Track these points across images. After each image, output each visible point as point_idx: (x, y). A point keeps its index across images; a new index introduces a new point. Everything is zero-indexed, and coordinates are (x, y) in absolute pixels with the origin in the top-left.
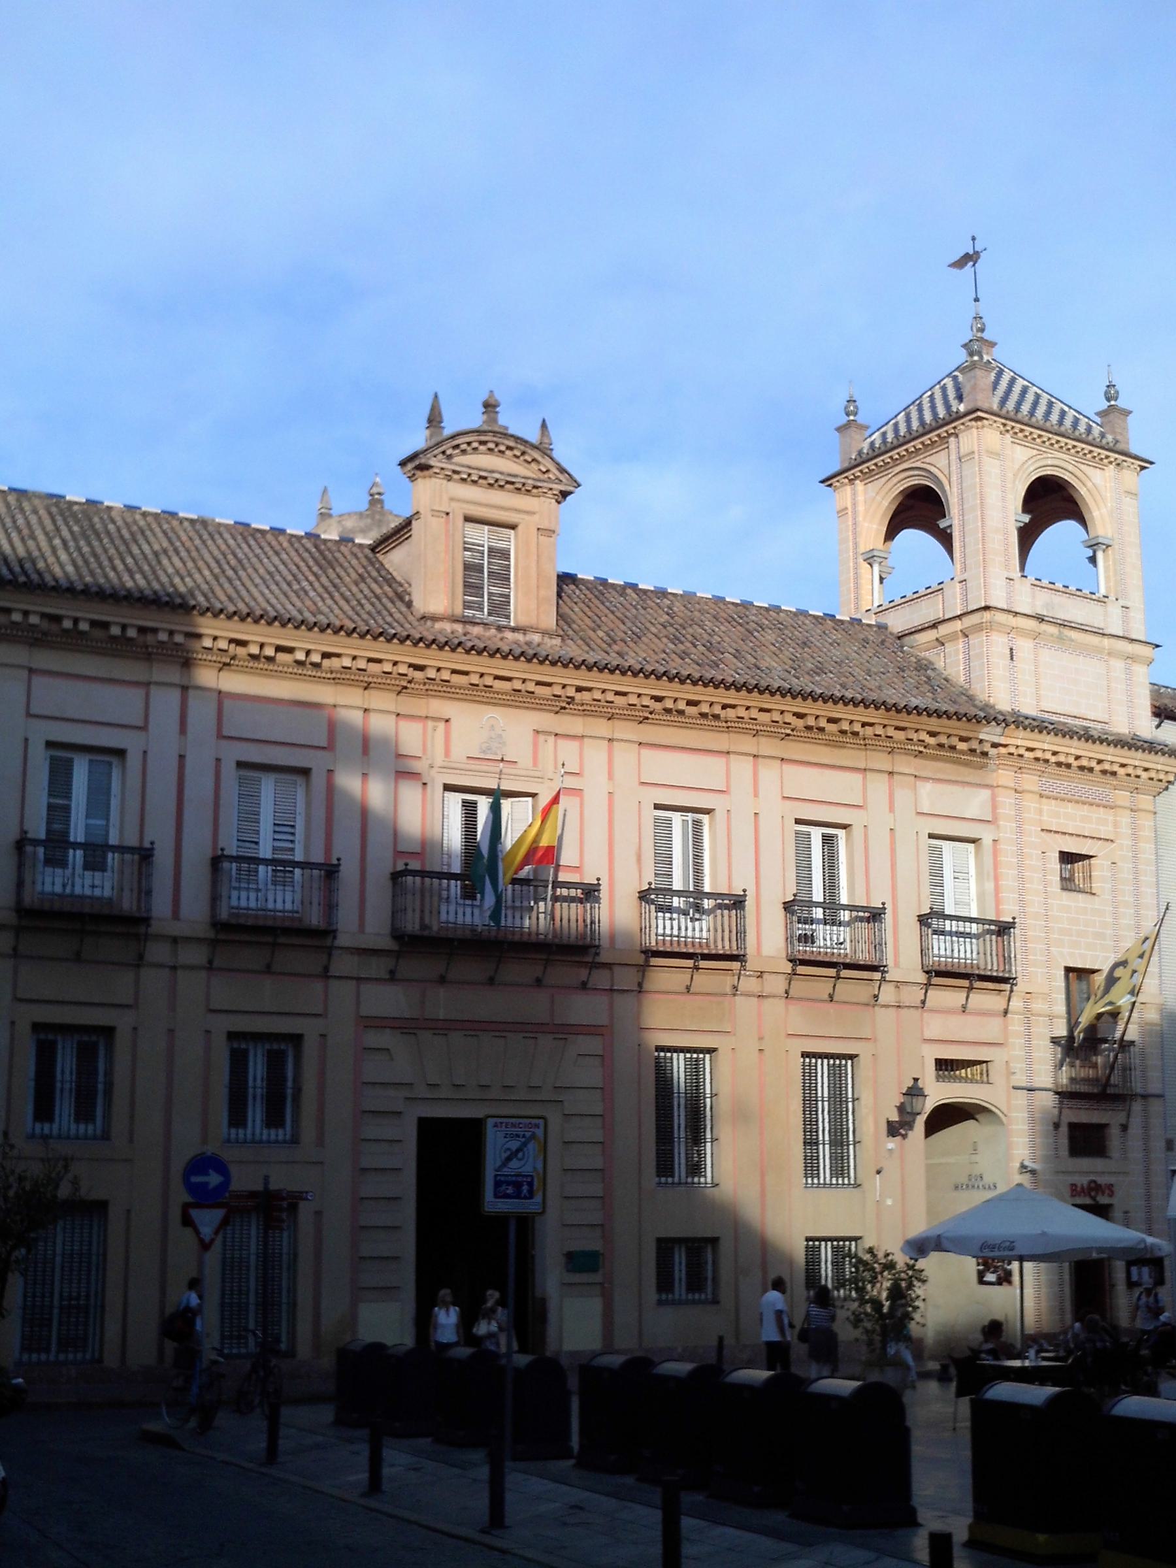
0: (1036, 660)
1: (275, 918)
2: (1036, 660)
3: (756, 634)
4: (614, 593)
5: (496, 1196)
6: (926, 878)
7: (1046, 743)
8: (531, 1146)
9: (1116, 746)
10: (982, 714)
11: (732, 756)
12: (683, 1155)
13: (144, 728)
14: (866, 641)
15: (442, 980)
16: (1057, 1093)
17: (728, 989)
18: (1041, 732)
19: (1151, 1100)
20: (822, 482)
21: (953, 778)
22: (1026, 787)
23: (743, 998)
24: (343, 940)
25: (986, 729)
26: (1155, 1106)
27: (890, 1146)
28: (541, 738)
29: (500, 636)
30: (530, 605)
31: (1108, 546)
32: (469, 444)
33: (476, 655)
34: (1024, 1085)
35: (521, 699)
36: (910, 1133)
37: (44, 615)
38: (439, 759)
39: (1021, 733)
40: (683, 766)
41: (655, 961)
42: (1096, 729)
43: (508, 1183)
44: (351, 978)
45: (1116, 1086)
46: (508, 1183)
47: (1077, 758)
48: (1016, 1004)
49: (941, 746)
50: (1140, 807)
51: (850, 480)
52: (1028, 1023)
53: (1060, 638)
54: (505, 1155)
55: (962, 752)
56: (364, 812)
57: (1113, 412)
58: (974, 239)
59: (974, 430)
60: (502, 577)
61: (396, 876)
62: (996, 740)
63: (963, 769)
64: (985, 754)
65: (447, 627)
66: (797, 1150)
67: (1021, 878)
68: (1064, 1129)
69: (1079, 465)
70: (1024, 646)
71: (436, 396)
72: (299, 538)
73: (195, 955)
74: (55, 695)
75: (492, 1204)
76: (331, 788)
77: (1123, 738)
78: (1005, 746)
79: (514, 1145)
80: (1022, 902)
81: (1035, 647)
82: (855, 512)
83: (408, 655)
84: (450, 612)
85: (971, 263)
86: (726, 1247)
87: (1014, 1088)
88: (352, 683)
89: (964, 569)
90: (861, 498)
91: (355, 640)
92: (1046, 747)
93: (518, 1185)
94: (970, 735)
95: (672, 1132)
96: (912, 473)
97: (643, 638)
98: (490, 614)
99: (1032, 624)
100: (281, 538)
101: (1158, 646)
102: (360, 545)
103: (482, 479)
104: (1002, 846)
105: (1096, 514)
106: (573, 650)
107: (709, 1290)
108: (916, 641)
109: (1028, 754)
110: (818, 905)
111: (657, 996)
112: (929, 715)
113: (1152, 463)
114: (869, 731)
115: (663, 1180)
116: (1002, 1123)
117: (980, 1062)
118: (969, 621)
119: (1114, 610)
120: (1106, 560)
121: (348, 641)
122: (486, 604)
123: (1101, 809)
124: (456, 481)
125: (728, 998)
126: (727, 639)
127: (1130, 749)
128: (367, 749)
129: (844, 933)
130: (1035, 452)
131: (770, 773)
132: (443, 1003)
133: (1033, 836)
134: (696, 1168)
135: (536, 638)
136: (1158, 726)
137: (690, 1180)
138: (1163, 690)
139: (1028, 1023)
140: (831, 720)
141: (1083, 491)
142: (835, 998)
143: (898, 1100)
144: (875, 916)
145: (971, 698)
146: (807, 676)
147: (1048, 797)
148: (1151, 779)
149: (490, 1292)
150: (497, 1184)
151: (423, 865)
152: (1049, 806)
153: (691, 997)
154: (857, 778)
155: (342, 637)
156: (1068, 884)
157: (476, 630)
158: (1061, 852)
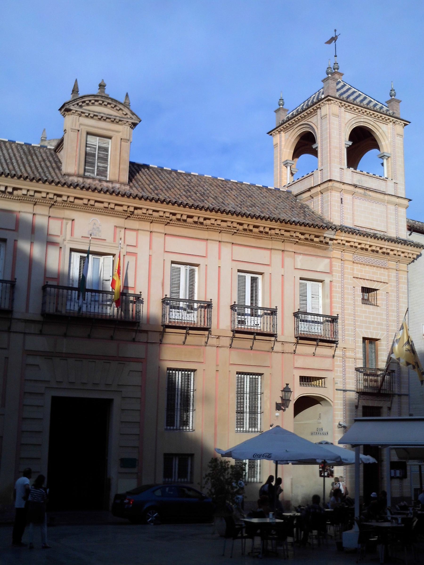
1: (70, 313)
3: (227, 191)
4: (165, 173)
6: (298, 298)
7: (355, 239)
9: (388, 241)
10: (325, 225)
11: (209, 241)
12: (179, 417)
14: (280, 197)
15: (65, 335)
16: (357, 392)
17: (203, 344)
18: (353, 234)
19: (403, 397)
20: (268, 133)
21: (314, 254)
22: (347, 258)
23: (210, 347)
24: (16, 315)
25: (327, 232)
26: (404, 399)
27: (277, 414)
28: (118, 230)
29: (100, 184)
30: (116, 172)
31: (389, 157)
32: (90, 101)
33: (89, 191)
34: (342, 388)
35: (108, 211)
36: (287, 409)
38: (68, 237)
39: (343, 234)
40: (185, 245)
41: (168, 330)
42: (379, 234)
44: (22, 333)
45: (385, 390)
47: (370, 246)
48: (339, 352)
49: (306, 239)
50: (401, 269)
51: (279, 132)
52: (344, 362)
53: (365, 195)
55: (317, 242)
56: (31, 260)
57: (393, 100)
58: (335, 31)
59: (327, 105)
60: (105, 159)
61: (44, 288)
62: (332, 237)
63: (316, 250)
64: (327, 243)
66: (234, 416)
67: (343, 298)
68: (360, 408)
69: (376, 122)
70: (347, 198)
71: (76, 80)
72: (21, 145)
73: (291, 348)
76: (15, 249)
77: (392, 238)
78: (336, 240)
80: (343, 309)
81: (353, 198)
82: (280, 146)
83: (53, 189)
84: (77, 173)
85: (334, 41)
86: (197, 459)
87: (337, 390)
88: (28, 202)
89: (322, 165)
90: (283, 139)
91: (28, 182)
92: (355, 241)
94: (319, 234)
95: (174, 406)
96: (305, 126)
97: (172, 190)
98: (97, 175)
99: (352, 188)
100: (13, 145)
101: (410, 200)
102: (50, 149)
103: (94, 116)
104: (334, 284)
105: (383, 143)
106: (135, 192)
107: (189, 478)
108: (302, 197)
109: (347, 244)
110: (248, 307)
111: (169, 346)
112: (301, 225)
113: (410, 122)
114: (273, 232)
115: (168, 427)
116: (331, 405)
117: (321, 378)
118: (323, 187)
119: (390, 184)
120: (388, 163)
121: (25, 182)
122: (96, 171)
123: (382, 269)
124: (83, 117)
125: (203, 347)
126: (213, 192)
127: (395, 243)
128: (34, 232)
129: (259, 320)
130: (355, 116)
131: (226, 250)
132: (65, 346)
134: (186, 423)
135: (117, 185)
136: (410, 235)
137: (181, 428)
138: (417, 223)
139: (344, 362)
140: (255, 227)
141: (378, 133)
142: (253, 348)
143: (280, 394)
144: (273, 312)
145: (322, 220)
146: (246, 208)
147: (357, 263)
148: (406, 257)
151: (58, 284)
152: (357, 267)
154: (268, 252)
155: (21, 181)
156: (365, 301)
157: (89, 181)
158: (362, 287)
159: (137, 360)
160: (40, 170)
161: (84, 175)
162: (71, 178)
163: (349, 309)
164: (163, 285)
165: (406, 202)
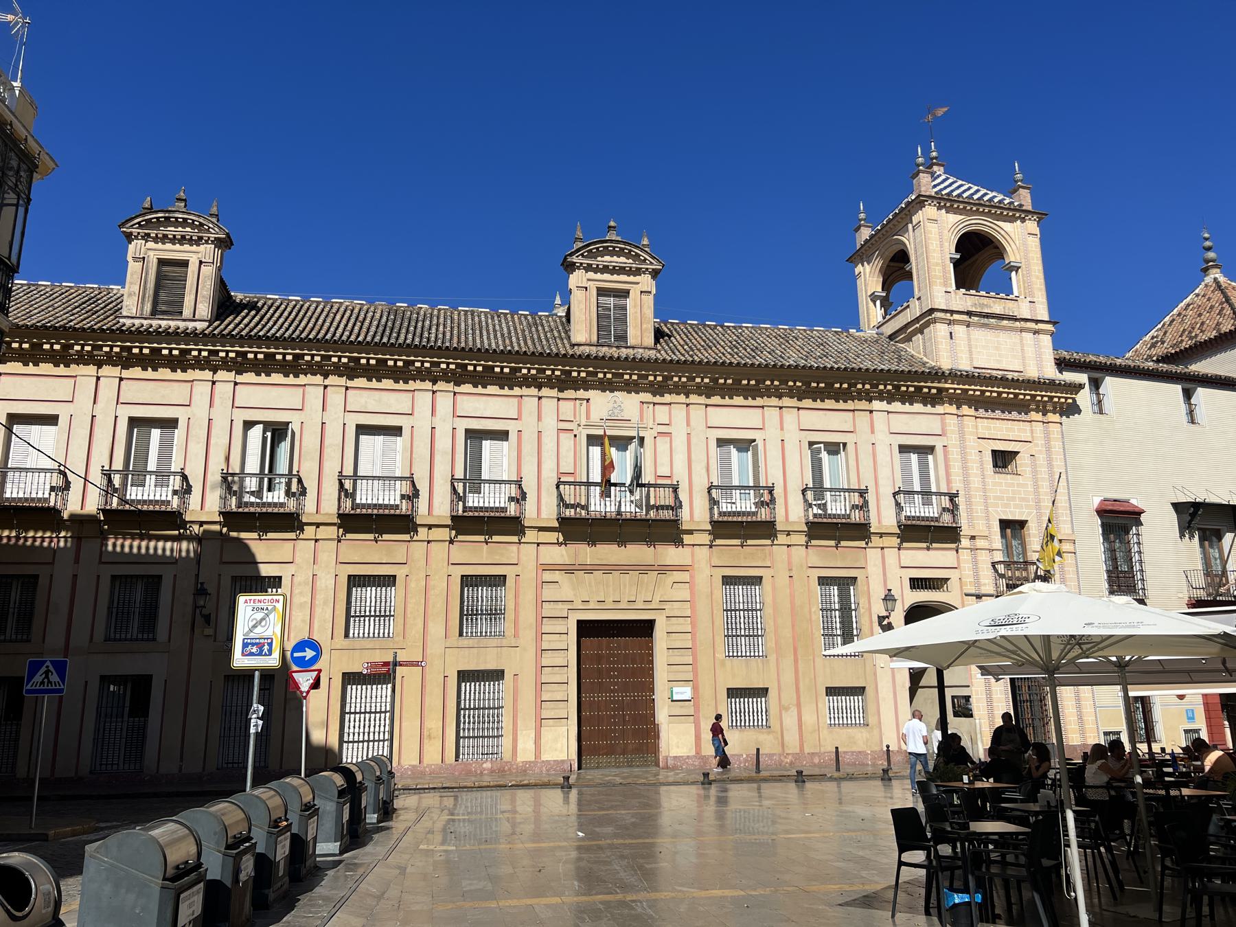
0: (969, 340)
2: (969, 340)
5: (243, 655)
8: (271, 616)
13: (52, 563)
34: (973, 592)
35: (631, 387)
37: (457, 364)
43: (253, 645)
46: (253, 645)
54: (251, 624)
65: (587, 350)
74: (246, 395)
75: (240, 660)
79: (259, 616)
80: (966, 481)
93: (260, 646)
99: (965, 317)
103: (605, 269)
131: (790, 417)
133: (971, 442)
149: (859, 269)
150: (245, 645)
153: (429, 659)
159: (682, 568)
160: (544, 342)
161: (456, 798)
162: (581, 348)
163: (975, 482)
164: (708, 470)
165: (1050, 327)
